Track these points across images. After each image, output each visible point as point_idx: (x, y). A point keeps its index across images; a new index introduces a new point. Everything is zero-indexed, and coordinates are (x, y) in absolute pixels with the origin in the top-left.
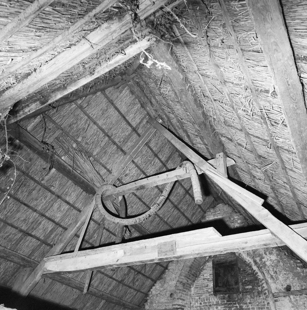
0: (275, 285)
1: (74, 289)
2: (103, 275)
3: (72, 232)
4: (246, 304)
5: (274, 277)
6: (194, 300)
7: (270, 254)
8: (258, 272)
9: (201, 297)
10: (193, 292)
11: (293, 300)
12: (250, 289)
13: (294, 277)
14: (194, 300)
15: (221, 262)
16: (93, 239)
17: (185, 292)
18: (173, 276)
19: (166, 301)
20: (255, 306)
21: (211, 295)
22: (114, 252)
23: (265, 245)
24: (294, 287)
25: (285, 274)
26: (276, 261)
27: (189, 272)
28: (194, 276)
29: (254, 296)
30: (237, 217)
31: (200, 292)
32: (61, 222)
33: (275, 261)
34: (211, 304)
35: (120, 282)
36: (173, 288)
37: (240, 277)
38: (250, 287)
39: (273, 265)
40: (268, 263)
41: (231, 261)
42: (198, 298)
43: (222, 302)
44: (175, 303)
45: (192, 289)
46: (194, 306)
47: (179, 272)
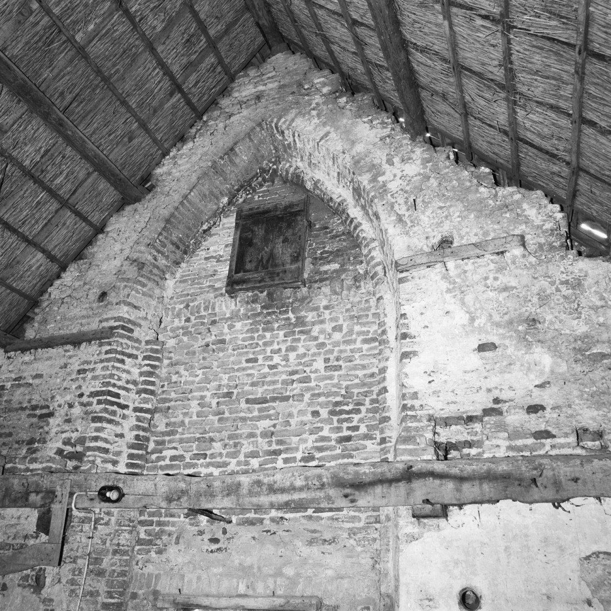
0: (406, 238)
4: (317, 309)
5: (405, 219)
6: (170, 313)
7: (403, 161)
8: (364, 222)
9: (191, 304)
10: (169, 293)
11: (453, 272)
12: (335, 271)
13: (466, 213)
14: (170, 313)
15: (260, 210)
17: (144, 285)
18: (116, 249)
19: (84, 313)
20: (342, 313)
21: (222, 295)
23: (396, 339)
24: (462, 238)
25: (441, 208)
26: (418, 177)
27: (160, 234)
28: (178, 247)
29: (342, 288)
30: (322, 79)
31: (192, 291)
33: (415, 178)
34: (217, 318)
36: (110, 278)
37: (311, 245)
38: (336, 266)
39: (408, 188)
40: (393, 186)
41: (291, 205)
42: (182, 306)
43: (247, 310)
44: (109, 316)
45: (170, 283)
46: (168, 328)
47: (135, 237)
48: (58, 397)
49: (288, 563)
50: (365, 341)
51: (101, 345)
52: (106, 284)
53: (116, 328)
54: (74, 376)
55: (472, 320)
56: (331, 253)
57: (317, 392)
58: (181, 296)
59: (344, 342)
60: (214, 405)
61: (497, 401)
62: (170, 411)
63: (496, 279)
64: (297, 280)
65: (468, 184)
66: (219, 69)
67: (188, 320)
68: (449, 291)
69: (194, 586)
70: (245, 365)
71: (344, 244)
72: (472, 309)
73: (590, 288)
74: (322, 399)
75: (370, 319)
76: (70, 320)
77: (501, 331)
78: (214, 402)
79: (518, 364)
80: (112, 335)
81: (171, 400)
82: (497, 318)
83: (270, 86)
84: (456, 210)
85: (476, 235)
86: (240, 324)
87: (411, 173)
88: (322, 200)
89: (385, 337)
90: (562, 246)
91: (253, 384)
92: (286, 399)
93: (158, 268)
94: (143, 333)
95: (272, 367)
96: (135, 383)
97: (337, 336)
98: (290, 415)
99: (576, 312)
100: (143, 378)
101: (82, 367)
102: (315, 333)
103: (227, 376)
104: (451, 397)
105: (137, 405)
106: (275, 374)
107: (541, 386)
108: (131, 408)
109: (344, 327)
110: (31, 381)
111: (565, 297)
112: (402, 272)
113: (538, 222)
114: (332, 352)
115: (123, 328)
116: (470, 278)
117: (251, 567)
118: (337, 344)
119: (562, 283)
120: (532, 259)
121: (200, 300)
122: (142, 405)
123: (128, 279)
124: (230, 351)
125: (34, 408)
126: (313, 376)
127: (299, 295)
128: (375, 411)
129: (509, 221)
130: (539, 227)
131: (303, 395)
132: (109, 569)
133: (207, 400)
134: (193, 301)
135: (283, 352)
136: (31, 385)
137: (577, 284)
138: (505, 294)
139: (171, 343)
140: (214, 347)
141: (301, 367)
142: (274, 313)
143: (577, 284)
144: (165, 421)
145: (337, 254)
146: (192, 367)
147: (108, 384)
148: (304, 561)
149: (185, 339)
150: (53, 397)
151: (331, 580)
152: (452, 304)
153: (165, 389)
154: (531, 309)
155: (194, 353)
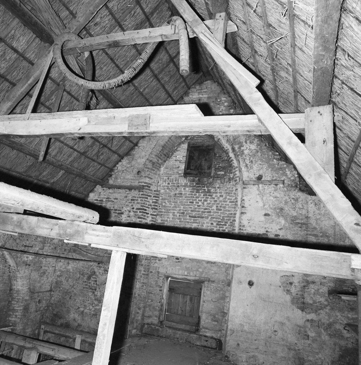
0: (248, 173)
1: (27, 156)
2: (62, 145)
3: (22, 90)
4: (215, 188)
5: (248, 166)
7: (250, 143)
9: (170, 178)
10: (162, 172)
11: (261, 188)
12: (222, 174)
16: (50, 101)
17: (154, 170)
19: (132, 178)
21: (181, 176)
22: (75, 119)
24: (265, 177)
25: (260, 164)
26: (255, 151)
27: (160, 152)
28: (166, 156)
30: (225, 99)
32: (7, 75)
33: (253, 151)
34: (179, 185)
35: (83, 154)
36: (141, 166)
38: (223, 173)
39: (251, 154)
40: (246, 152)
41: (208, 146)
42: (166, 178)
43: (190, 183)
45: (162, 169)
46: (161, 185)
47: (150, 151)
48: (124, 208)
49: (200, 268)
50: (230, 202)
51: (139, 191)
52: (140, 168)
53: (145, 186)
54: (130, 201)
55: (264, 205)
56: (222, 167)
57: (213, 217)
58: (167, 174)
59: (223, 201)
60: (178, 216)
61: (267, 231)
62: (162, 216)
63: (273, 193)
64: (209, 176)
65: (270, 157)
66: (185, 86)
67: (169, 184)
68: (258, 194)
69: (171, 271)
70: (189, 203)
71: (227, 164)
72: (265, 202)
73: (300, 201)
74: (214, 219)
75: (233, 195)
76: (127, 179)
77: (272, 211)
78: (178, 215)
79: (275, 222)
80: (144, 189)
81: (162, 212)
82: (271, 206)
83: (205, 96)
84: (265, 166)
85: (270, 177)
86: (188, 188)
87: (253, 149)
88: (220, 146)
89: (237, 203)
90: (295, 186)
91: (192, 211)
92: (203, 217)
93: (159, 164)
94: (153, 188)
95: (198, 206)
96: (151, 205)
97: (221, 199)
98: (204, 223)
99: (294, 209)
100: (153, 204)
101: (133, 198)
102: (214, 196)
103: (183, 206)
104: (254, 228)
105: (152, 213)
106: (199, 209)
107: (280, 229)
108: (150, 214)
109: (224, 196)
110: (113, 200)
111: (292, 203)
112: (245, 185)
113: (289, 177)
114: (219, 204)
115: (148, 186)
116: (266, 191)
117: (189, 268)
118: (221, 201)
119: (292, 199)
120: (285, 189)
121: (173, 177)
122: (153, 213)
123: (149, 168)
124: (184, 198)
125: (116, 210)
126: (212, 211)
127: (209, 181)
128: (231, 226)
129: (281, 174)
130: (290, 178)
131: (208, 217)
132: (144, 264)
133: (176, 214)
134: (171, 177)
135: (202, 201)
136: (113, 201)
137: (296, 200)
138: (275, 199)
139: (162, 191)
140: (178, 195)
141: (208, 207)
142: (200, 186)
143: (296, 200)
144: (161, 219)
145: (224, 168)
146: (170, 201)
147: (143, 206)
148: (205, 268)
149: (168, 190)
150: (122, 207)
151: (213, 274)
152: (259, 199)
153: (160, 207)
154: (282, 205)
155: (171, 196)
